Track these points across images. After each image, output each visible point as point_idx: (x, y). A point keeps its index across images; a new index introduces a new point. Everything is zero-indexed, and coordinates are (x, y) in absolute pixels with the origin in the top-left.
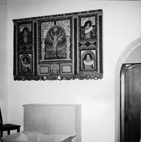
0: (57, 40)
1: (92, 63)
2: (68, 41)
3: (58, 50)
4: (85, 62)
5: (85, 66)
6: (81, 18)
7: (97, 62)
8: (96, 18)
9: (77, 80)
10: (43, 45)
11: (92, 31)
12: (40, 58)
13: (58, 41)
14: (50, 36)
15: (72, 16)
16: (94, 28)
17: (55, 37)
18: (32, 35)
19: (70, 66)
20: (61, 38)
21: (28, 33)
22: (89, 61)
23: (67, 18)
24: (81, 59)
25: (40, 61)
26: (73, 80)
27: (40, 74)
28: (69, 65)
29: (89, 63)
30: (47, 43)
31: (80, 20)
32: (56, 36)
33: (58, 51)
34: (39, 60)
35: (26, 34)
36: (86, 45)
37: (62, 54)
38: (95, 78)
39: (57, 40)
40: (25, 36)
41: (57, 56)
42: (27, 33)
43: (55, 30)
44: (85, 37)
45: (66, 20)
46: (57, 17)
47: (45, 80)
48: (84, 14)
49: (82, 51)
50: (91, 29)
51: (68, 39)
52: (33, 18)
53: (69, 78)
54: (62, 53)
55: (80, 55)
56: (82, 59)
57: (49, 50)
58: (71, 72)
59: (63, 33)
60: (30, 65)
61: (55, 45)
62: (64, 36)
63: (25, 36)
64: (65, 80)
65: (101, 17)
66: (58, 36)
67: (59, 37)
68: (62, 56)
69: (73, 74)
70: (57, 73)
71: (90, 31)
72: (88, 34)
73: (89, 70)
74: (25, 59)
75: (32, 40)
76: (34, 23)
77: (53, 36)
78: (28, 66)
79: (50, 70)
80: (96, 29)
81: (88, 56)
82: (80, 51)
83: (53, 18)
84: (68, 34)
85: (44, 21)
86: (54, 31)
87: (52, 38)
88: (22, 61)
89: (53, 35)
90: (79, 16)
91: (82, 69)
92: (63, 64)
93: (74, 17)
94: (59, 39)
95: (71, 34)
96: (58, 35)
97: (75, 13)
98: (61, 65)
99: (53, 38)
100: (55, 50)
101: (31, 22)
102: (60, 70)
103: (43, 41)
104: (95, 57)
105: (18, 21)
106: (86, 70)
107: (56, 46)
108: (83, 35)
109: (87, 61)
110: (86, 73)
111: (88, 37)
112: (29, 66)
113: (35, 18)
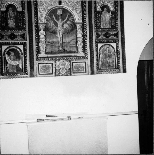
0: (63, 27)
3: (64, 41)
10: (42, 32)
12: (38, 51)
13: (64, 29)
14: (52, 21)
16: (113, 15)
17: (60, 23)
20: (68, 24)
21: (15, 13)
25: (38, 56)
28: (83, 62)
30: (47, 31)
32: (60, 21)
33: (64, 43)
34: (37, 55)
35: (12, 15)
36: (105, 37)
37: (70, 47)
39: (63, 27)
41: (64, 49)
43: (59, 12)
49: (22, 46)
51: (79, 27)
54: (71, 46)
55: (97, 49)
57: (51, 41)
60: (21, 62)
61: (60, 34)
62: (73, 22)
63: (10, 17)
66: (64, 21)
67: (66, 22)
68: (71, 49)
74: (11, 53)
77: (56, 20)
78: (18, 64)
79: (56, 69)
82: (97, 43)
84: (77, 18)
87: (54, 24)
88: (7, 56)
89: (56, 19)
91: (100, 67)
94: (66, 25)
96: (63, 21)
98: (72, 61)
99: (56, 24)
100: (60, 41)
102: (70, 69)
103: (42, 27)
104: (116, 52)
107: (61, 36)
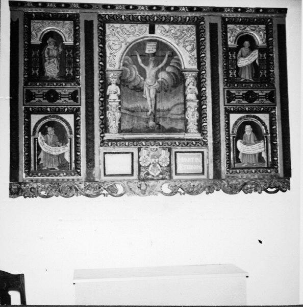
0: (157, 78)
1: (259, 148)
2: (191, 86)
3: (159, 106)
4: (240, 145)
5: (240, 157)
6: (229, 26)
7: (274, 147)
8: (267, 29)
9: (219, 195)
10: (113, 90)
11: (257, 62)
12: (105, 128)
13: (158, 82)
14: (134, 66)
15: (206, 14)
16: (263, 54)
17: (150, 70)
18: (76, 56)
19: (198, 154)
20: (168, 73)
21: (60, 49)
22: (250, 144)
23: (189, 20)
24: (231, 138)
25: (104, 136)
26: (207, 193)
27: (103, 178)
29: (250, 149)
31: (225, 31)
32: (151, 65)
33: (159, 111)
34: (102, 135)
36: (57, 94)
37: (171, 119)
38: (269, 190)
39: (157, 78)
40: (50, 57)
41: (158, 124)
42: (57, 50)
44: (238, 76)
45: (183, 24)
46: (159, 13)
47: (121, 195)
48: (155, 13)
50: (254, 56)
51: (190, 79)
52: (82, 6)
53: (195, 189)
54: (173, 117)
55: (228, 124)
56: (234, 137)
57: (130, 106)
58: (203, 173)
59: (173, 60)
60: (68, 148)
61: (149, 92)
62: (178, 69)
64: (184, 194)
65: (282, 29)
66: (160, 66)
67: (163, 69)
68: (174, 125)
69: (211, 177)
70: (161, 174)
71: (253, 60)
72: (247, 70)
73: (253, 168)
74: (49, 129)
75: (76, 72)
76: (86, 22)
77: (142, 65)
79: (140, 166)
80: (270, 59)
81: (248, 127)
82: (228, 112)
83: (146, 14)
85: (109, 22)
86: (147, 52)
89: (143, 61)
90: (223, 19)
92: (179, 149)
93: (208, 20)
95: (199, 66)
96: (158, 65)
97: (215, 9)
98: (174, 150)
99: (143, 73)
100: (150, 107)
101: (74, 19)
102: (169, 166)
103: (113, 78)
104: (269, 132)
105: (28, 7)
106: (244, 166)
107: (153, 96)
108: (235, 72)
109: (245, 144)
110: (245, 176)
111: (247, 78)
112: (65, 150)
113: (90, 6)
